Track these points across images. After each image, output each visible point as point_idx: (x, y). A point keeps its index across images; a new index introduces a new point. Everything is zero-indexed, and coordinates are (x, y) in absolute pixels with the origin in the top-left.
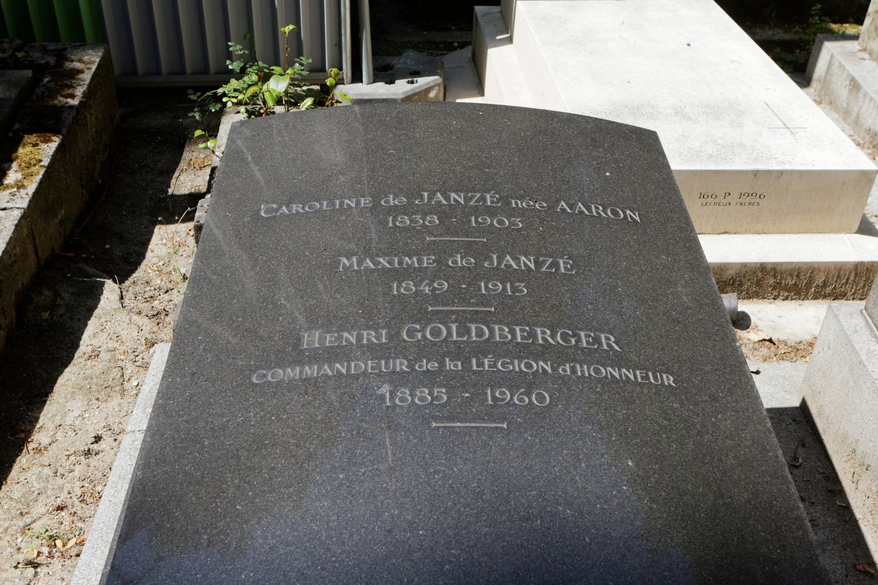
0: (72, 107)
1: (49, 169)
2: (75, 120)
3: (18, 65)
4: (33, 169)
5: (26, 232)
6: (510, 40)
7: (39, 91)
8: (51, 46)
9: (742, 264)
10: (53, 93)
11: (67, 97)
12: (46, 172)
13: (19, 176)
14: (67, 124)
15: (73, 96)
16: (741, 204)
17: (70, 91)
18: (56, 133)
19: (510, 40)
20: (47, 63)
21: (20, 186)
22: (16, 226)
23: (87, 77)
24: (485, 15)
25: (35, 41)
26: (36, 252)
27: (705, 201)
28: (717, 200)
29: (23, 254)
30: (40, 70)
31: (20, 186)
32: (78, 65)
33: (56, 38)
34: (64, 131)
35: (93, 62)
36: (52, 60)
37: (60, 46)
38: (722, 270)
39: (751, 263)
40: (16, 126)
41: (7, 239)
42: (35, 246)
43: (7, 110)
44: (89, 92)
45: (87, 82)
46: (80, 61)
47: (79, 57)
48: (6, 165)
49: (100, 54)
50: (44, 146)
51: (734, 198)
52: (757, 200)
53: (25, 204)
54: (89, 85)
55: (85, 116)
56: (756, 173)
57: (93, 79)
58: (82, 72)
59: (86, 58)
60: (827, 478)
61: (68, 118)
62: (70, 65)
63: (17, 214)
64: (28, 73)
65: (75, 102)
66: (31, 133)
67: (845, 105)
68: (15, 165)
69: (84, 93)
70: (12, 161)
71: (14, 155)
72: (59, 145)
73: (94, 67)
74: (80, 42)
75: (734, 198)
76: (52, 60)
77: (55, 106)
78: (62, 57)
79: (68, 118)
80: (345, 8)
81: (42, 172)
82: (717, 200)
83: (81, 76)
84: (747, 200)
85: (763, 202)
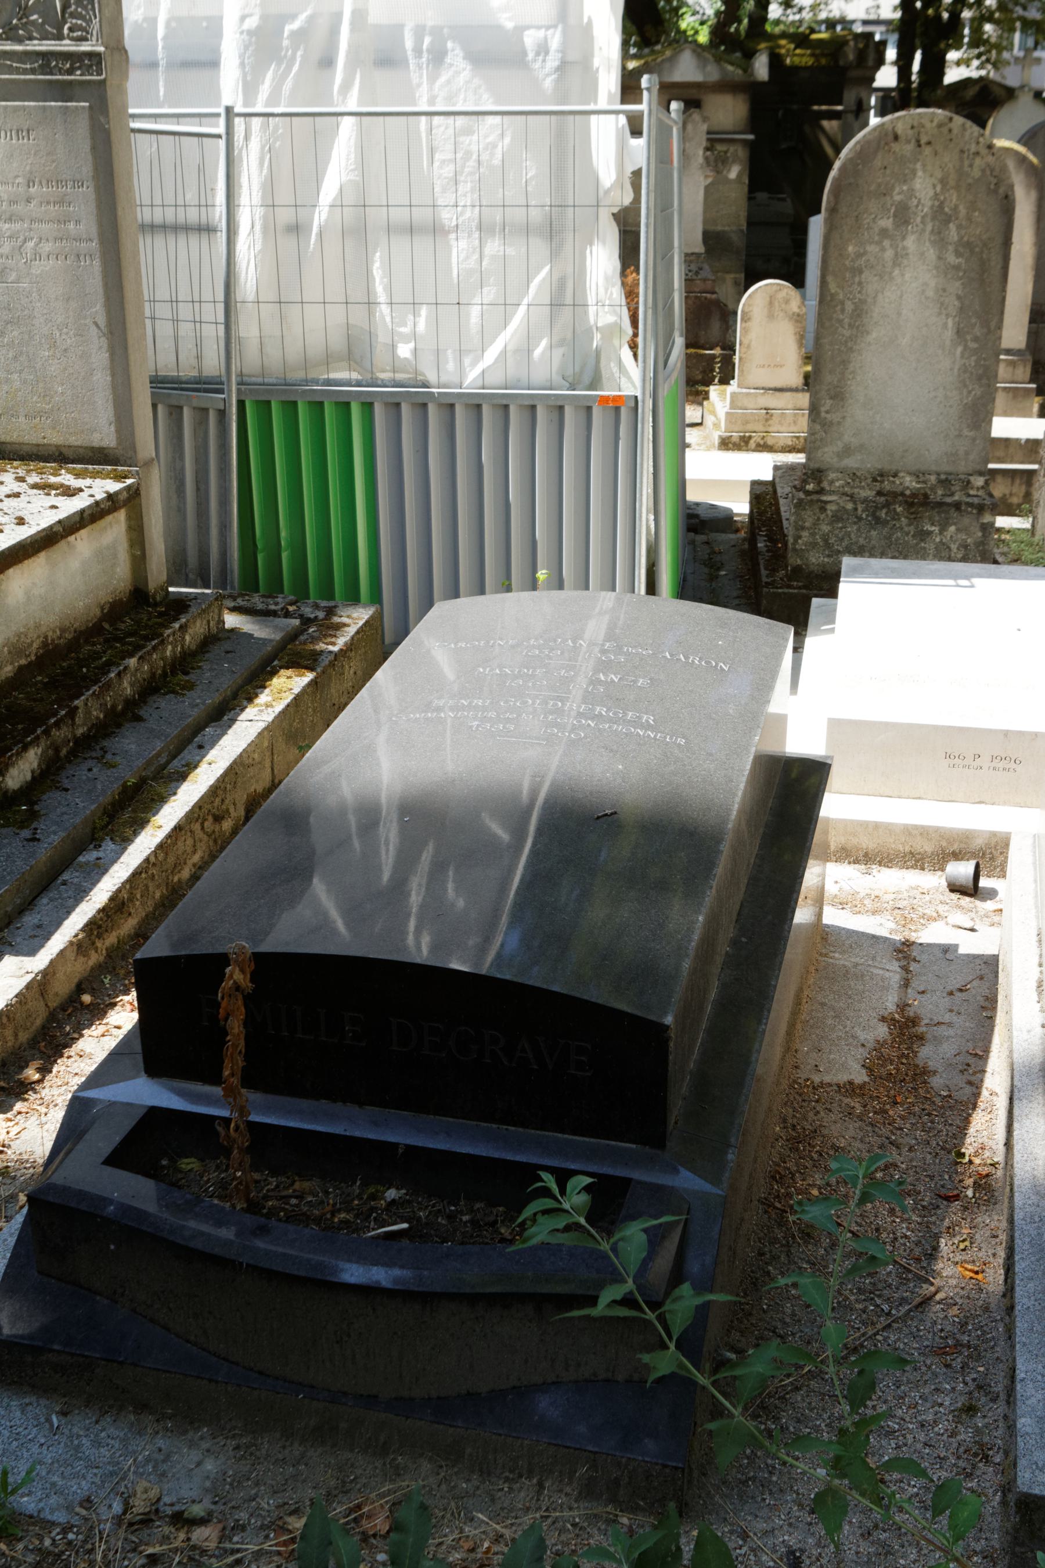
0: (331, 652)
1: (297, 699)
2: (332, 664)
3: (287, 615)
4: (283, 694)
5: (266, 744)
6: (832, 630)
7: (302, 638)
8: (324, 603)
9: (990, 832)
10: (314, 640)
11: (327, 644)
12: (295, 698)
13: (270, 699)
14: (323, 665)
15: (333, 644)
16: (994, 769)
17: (333, 640)
18: (311, 669)
19: (832, 630)
20: (316, 617)
21: (268, 705)
22: (259, 734)
23: (352, 630)
24: (819, 607)
25: (308, 598)
26: (272, 769)
27: (952, 762)
28: (966, 762)
29: (260, 763)
30: (307, 622)
31: (268, 705)
32: (345, 620)
33: (331, 596)
34: (319, 670)
35: (361, 619)
36: (321, 615)
37: (332, 604)
38: (967, 837)
39: (1000, 833)
40: (276, 663)
41: (249, 741)
42: (272, 762)
43: (269, 649)
44: (351, 644)
45: (352, 633)
46: (348, 617)
47: (349, 613)
48: (259, 690)
49: (371, 612)
50: (298, 679)
51: (985, 761)
52: (1012, 765)
53: (270, 719)
54: (352, 638)
55: (343, 666)
56: (1006, 733)
57: (358, 632)
58: (348, 626)
59: (355, 615)
60: (987, 998)
61: (325, 661)
62: (336, 619)
63: (262, 725)
64: (296, 622)
65: (336, 649)
66: (288, 668)
67: (50, 225)
68: (267, 691)
69: (346, 644)
70: (265, 687)
71: (268, 683)
72: (312, 680)
73: (361, 623)
74: (354, 599)
75: (985, 761)
76: (321, 615)
77: (315, 651)
78: (331, 612)
79: (325, 661)
80: (640, 582)
81: (292, 697)
82: (966, 762)
83: (346, 629)
84: (1001, 765)
85: (1019, 768)
